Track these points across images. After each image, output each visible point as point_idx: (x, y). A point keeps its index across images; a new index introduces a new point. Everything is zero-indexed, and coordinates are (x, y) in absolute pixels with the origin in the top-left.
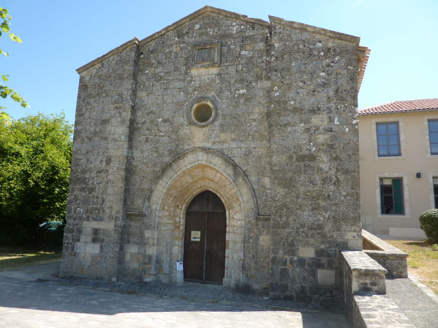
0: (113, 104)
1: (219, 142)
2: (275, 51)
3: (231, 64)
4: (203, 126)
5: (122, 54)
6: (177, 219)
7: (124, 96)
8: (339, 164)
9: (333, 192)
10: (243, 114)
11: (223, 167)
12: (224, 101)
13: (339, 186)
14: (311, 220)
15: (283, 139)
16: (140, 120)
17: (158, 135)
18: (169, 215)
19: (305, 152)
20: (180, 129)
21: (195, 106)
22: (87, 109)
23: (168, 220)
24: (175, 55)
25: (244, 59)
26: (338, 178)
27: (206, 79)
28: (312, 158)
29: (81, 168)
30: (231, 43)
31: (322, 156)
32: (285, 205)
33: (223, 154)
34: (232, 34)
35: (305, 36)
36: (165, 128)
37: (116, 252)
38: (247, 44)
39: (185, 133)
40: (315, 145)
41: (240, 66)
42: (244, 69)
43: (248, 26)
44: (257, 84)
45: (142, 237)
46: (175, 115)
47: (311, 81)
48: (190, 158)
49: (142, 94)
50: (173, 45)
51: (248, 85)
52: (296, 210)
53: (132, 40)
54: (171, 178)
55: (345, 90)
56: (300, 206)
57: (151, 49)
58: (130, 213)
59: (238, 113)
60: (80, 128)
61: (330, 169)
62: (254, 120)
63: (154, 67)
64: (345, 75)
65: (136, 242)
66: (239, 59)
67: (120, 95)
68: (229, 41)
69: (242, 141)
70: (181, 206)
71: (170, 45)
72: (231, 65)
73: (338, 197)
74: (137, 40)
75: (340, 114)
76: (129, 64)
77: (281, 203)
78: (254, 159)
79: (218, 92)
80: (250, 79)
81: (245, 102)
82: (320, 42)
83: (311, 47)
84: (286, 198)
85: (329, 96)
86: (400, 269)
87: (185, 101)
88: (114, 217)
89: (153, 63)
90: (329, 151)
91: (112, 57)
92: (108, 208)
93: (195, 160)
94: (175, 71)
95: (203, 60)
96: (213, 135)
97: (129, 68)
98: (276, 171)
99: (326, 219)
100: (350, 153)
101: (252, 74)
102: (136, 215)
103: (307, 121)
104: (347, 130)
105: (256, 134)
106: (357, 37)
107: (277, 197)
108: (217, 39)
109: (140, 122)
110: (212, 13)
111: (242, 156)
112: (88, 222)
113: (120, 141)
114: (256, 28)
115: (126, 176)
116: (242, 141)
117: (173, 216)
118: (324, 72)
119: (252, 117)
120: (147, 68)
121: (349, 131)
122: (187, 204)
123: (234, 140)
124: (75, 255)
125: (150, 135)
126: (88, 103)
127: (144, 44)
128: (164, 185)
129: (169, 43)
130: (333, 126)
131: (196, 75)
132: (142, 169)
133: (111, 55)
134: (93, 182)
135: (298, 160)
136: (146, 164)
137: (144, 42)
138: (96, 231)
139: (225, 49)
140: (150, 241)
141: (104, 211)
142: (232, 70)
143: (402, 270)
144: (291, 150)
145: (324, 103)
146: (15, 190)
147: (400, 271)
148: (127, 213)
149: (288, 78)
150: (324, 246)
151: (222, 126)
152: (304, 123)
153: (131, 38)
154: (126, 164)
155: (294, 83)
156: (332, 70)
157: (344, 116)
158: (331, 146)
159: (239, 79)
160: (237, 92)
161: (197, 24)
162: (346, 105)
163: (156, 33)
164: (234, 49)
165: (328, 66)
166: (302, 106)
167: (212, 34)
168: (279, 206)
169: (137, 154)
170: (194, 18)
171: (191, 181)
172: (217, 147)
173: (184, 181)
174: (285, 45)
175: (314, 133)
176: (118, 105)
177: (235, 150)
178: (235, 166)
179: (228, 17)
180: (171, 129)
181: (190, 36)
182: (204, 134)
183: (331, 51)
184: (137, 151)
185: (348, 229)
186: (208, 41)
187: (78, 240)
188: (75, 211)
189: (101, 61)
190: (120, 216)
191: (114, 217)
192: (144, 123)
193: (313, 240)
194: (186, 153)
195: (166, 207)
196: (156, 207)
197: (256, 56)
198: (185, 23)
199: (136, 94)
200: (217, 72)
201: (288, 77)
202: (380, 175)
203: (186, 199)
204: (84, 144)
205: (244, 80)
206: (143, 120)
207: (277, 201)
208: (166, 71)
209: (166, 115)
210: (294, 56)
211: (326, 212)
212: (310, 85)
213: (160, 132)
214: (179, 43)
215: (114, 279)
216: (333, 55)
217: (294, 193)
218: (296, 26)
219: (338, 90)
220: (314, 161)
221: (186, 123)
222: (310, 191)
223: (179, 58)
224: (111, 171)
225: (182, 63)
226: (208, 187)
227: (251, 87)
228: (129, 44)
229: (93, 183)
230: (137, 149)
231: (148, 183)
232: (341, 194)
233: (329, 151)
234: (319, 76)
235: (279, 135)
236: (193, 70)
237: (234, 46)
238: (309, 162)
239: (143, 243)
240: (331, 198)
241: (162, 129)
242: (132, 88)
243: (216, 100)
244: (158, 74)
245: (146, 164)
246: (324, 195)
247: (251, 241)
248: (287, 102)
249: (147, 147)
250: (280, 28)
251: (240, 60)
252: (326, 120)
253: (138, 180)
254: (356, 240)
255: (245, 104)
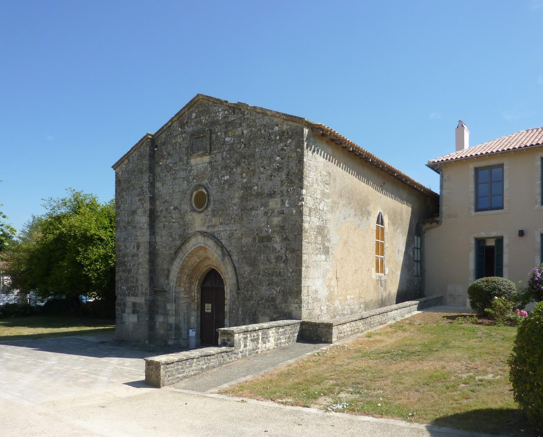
0: (138, 196)
1: (211, 226)
2: (244, 138)
3: (219, 151)
4: (200, 212)
5: (141, 149)
6: (193, 293)
7: (144, 189)
8: (288, 244)
9: (283, 269)
10: (228, 198)
11: (215, 248)
12: (214, 188)
13: (287, 264)
14: (267, 293)
15: (249, 223)
16: (159, 209)
17: (171, 221)
18: (185, 290)
19: (264, 234)
20: (185, 215)
21: (195, 193)
22: (122, 202)
23: (184, 294)
24: (179, 146)
25: (227, 146)
26: (286, 257)
27: (201, 167)
28: (269, 239)
29: (122, 253)
30: (218, 130)
31: (276, 237)
32: (250, 281)
33: (214, 237)
34: (218, 121)
35: (267, 120)
36: (176, 214)
37: (147, 321)
38: (230, 130)
39: (189, 219)
40: (272, 227)
41: (225, 152)
42: (228, 156)
43: (230, 111)
44: (237, 170)
45: (165, 309)
46: (181, 203)
47: (269, 166)
48: (193, 241)
49: (158, 185)
50: (178, 135)
51: (230, 171)
52: (258, 285)
53: (146, 136)
54: (182, 259)
55: (294, 173)
56: (260, 282)
57: (163, 141)
58: (156, 289)
59: (224, 198)
60: (119, 218)
61: (281, 249)
62: (235, 204)
63: (166, 159)
64: (295, 158)
65: (162, 313)
66: (224, 146)
67: (141, 188)
68: (216, 128)
69: (227, 224)
70: (195, 282)
71: (176, 136)
72: (218, 153)
73: (286, 274)
74: (150, 135)
75: (290, 197)
76: (146, 159)
77: (248, 279)
78: (235, 240)
79: (210, 179)
80: (232, 165)
81: (228, 188)
82: (277, 126)
83: (270, 131)
84: (251, 275)
85: (282, 179)
86: (327, 336)
87: (188, 190)
88: (144, 293)
89: (164, 154)
90: (281, 233)
91: (134, 153)
92: (140, 286)
93: (196, 243)
94: (180, 161)
95: (198, 150)
96: (207, 220)
97: (146, 162)
98: (245, 251)
99: (277, 293)
100: (296, 233)
101: (233, 160)
102: (161, 291)
103: (265, 205)
104: (294, 211)
105: (237, 218)
106: (302, 118)
107: (245, 274)
108: (208, 127)
109: (159, 211)
110: (204, 100)
111: (227, 238)
112: (129, 297)
113: (144, 229)
114: (236, 112)
115: (150, 259)
116: (227, 224)
117: (189, 291)
118: (279, 156)
119: (234, 202)
120: (161, 160)
121: (296, 213)
122: (200, 280)
123: (221, 224)
124: (123, 323)
125: (166, 222)
126: (122, 196)
127: (157, 137)
128: (177, 266)
129: (175, 134)
130: (284, 209)
131: (194, 164)
132: (163, 252)
133: (133, 151)
134: (130, 265)
135: (260, 241)
136: (165, 247)
137: (157, 135)
138: (134, 304)
139: (214, 136)
140: (171, 312)
141: (138, 289)
142: (219, 157)
143: (328, 337)
144: (255, 232)
145: (278, 187)
146: (101, 270)
147: (327, 337)
148: (155, 289)
149: (253, 165)
150: (276, 315)
151: (213, 211)
152: (264, 207)
153: (144, 135)
154: (149, 248)
155: (257, 169)
156: (285, 154)
157: (292, 198)
158: (283, 228)
159: (224, 166)
160: (222, 178)
161: (193, 113)
162: (295, 188)
163: (164, 126)
164: (221, 135)
165: (282, 149)
166: (263, 191)
167: (205, 122)
168: (247, 282)
169: (158, 239)
170: (191, 107)
171: (199, 260)
172: (210, 230)
173: (193, 261)
174: (251, 131)
175: (271, 215)
176: (140, 197)
177: (222, 233)
178: (222, 247)
179: (216, 103)
180: (179, 216)
181: (189, 125)
182: (202, 219)
183: (285, 134)
184: (158, 236)
185: (292, 301)
186: (202, 129)
187: (124, 312)
188: (121, 289)
189: (128, 157)
190: (147, 292)
191: (144, 293)
192: (161, 211)
193: (268, 310)
194: (189, 237)
195: (182, 284)
196: (173, 284)
197: (236, 141)
198: (185, 112)
199: (155, 186)
200: (209, 160)
201: (253, 163)
202: (475, 235)
203: (198, 276)
204: (122, 233)
205: (228, 167)
206: (161, 209)
207: (245, 277)
208: (174, 162)
209: (176, 203)
210: (257, 141)
211: (278, 287)
212: (268, 170)
213: (172, 219)
214: (182, 133)
215: (147, 342)
216: (287, 138)
217: (256, 271)
218: (259, 111)
219: (289, 173)
220: (270, 242)
221: (189, 210)
222: (267, 269)
223: (182, 149)
224: (140, 255)
225: (184, 154)
226: (212, 265)
227: (233, 172)
228: (144, 139)
229: (130, 266)
230: (158, 235)
231: (167, 264)
232: (288, 270)
233: (281, 233)
234: (275, 161)
235: (246, 219)
236: (192, 160)
237: (220, 133)
238: (267, 243)
239: (166, 314)
240: (282, 274)
241: (174, 216)
242: (149, 180)
243: (209, 187)
244: (168, 165)
245: (165, 247)
246: (277, 272)
247: (234, 311)
248: (252, 188)
249: (164, 232)
250: (248, 114)
251: (225, 147)
252: (280, 203)
253: (160, 261)
254: (298, 310)
255: (228, 189)
